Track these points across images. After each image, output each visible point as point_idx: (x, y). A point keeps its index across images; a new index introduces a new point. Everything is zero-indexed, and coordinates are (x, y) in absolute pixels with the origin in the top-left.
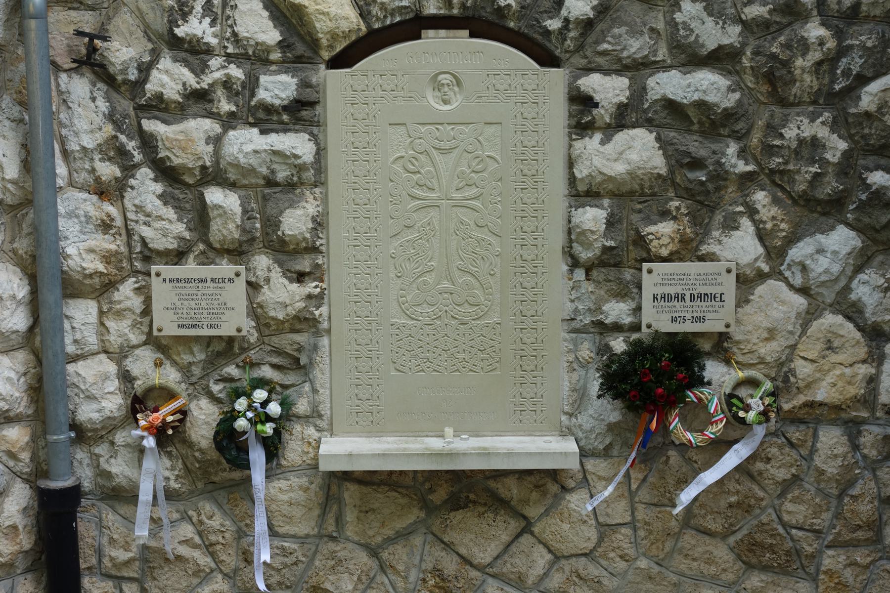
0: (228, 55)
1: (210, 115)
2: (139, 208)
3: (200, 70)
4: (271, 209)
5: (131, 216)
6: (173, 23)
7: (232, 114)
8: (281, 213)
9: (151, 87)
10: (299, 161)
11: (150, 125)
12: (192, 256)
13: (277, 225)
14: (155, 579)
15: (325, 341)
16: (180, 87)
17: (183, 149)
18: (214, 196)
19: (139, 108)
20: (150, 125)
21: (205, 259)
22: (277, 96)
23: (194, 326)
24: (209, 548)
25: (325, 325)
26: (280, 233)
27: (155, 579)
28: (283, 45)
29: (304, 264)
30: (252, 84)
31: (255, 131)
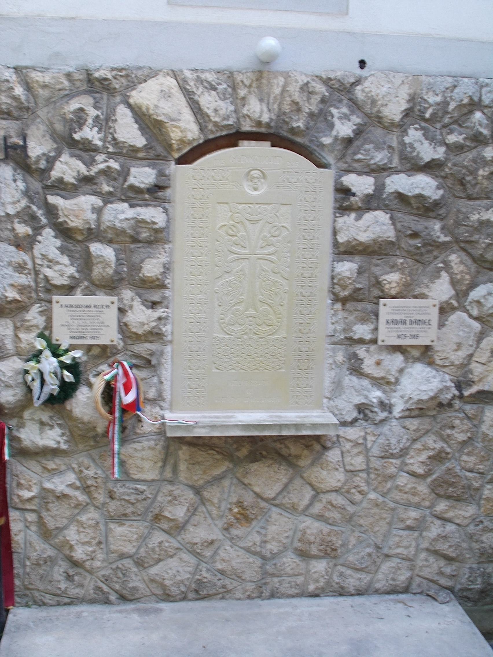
0: (109, 153)
1: (95, 193)
2: (44, 256)
3: (90, 163)
4: (136, 258)
5: (38, 261)
6: (72, 130)
7: (110, 193)
8: (142, 261)
9: (55, 174)
10: (155, 226)
11: (52, 199)
12: (79, 290)
13: (140, 269)
14: (48, 510)
15: (168, 349)
16: (75, 174)
17: (77, 216)
18: (96, 248)
19: (46, 187)
20: (52, 199)
21: (88, 292)
22: (143, 182)
23: (81, 338)
24: (86, 489)
25: (169, 338)
26: (141, 275)
27: (48, 510)
28: (147, 148)
29: (156, 297)
30: (125, 173)
31: (126, 205)
